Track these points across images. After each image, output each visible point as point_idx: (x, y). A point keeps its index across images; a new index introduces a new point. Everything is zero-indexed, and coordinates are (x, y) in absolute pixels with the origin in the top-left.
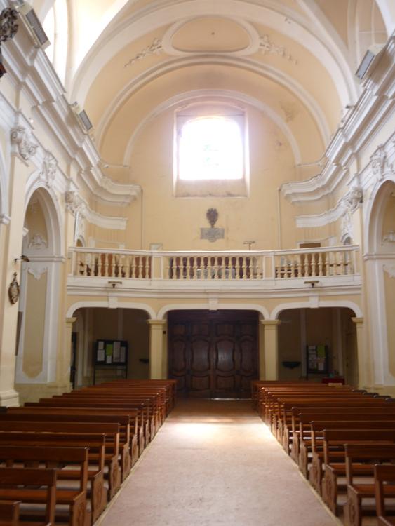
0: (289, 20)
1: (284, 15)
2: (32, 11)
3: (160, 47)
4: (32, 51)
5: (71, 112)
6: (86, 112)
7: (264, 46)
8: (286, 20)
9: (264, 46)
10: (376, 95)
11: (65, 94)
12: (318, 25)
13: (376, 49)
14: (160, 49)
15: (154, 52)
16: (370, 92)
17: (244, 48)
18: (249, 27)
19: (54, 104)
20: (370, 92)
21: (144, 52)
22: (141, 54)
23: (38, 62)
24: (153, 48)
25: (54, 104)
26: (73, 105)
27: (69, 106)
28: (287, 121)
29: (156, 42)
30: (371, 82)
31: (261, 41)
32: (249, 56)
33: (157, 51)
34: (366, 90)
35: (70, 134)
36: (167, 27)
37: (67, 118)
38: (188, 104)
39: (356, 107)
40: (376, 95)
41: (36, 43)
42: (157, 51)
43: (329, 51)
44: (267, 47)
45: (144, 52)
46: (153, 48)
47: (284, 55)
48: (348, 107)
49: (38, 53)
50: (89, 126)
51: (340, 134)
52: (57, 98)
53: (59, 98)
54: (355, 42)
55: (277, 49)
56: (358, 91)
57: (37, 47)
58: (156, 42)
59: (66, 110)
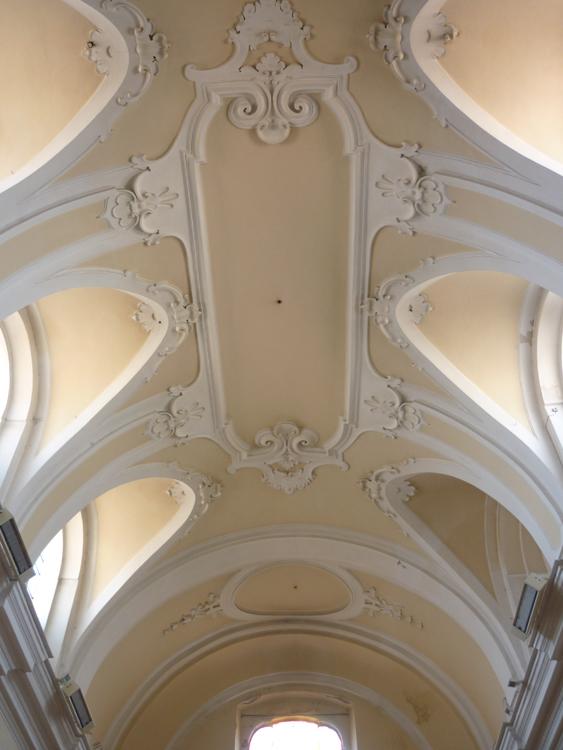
0: (403, 563)
1: (396, 556)
2: (12, 521)
3: (218, 606)
4: (5, 584)
5: (58, 693)
6: (82, 692)
7: (371, 603)
8: (399, 563)
9: (371, 603)
10: (553, 658)
11: (50, 659)
12: (429, 548)
13: (538, 582)
14: (216, 609)
15: (208, 613)
16: (543, 654)
17: (339, 610)
18: (347, 577)
19: (28, 674)
20: (543, 654)
21: (193, 613)
22: (189, 616)
23: (11, 602)
24: (207, 607)
25: (30, 676)
26: (61, 681)
27: (55, 683)
28: (419, 723)
29: (211, 598)
30: (542, 637)
31: (366, 597)
32: (351, 620)
33: (212, 611)
34: (536, 651)
35: (51, 732)
36: (230, 576)
37: (50, 705)
38: (260, 695)
39: (525, 683)
40: (553, 658)
41: (13, 574)
42: (212, 611)
43: (472, 609)
44: (376, 605)
45: (193, 613)
46: (207, 607)
47: (402, 616)
48: (512, 684)
49: (14, 588)
50: (85, 720)
51: (508, 735)
52: (36, 665)
53: (39, 665)
54: (505, 590)
55: (391, 607)
56: (521, 655)
57: (14, 580)
58: (211, 598)
59: (50, 689)
